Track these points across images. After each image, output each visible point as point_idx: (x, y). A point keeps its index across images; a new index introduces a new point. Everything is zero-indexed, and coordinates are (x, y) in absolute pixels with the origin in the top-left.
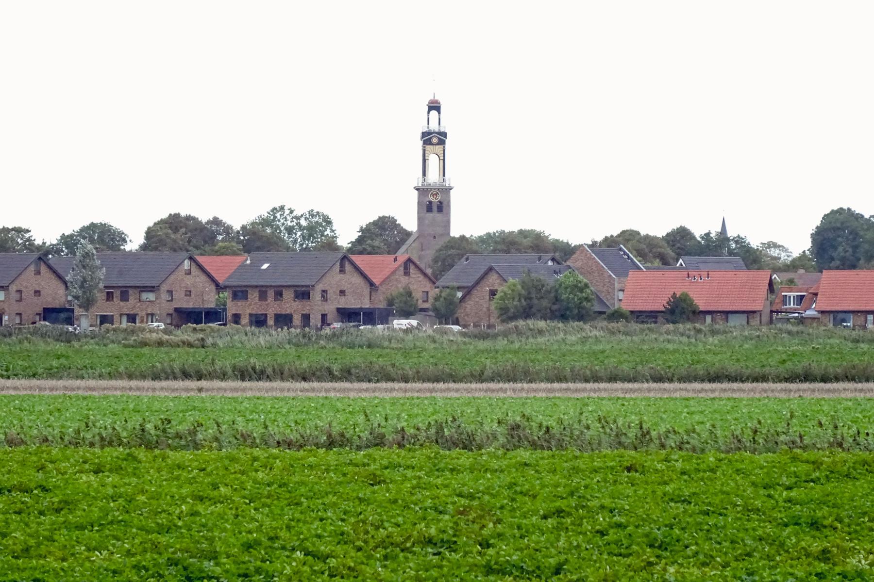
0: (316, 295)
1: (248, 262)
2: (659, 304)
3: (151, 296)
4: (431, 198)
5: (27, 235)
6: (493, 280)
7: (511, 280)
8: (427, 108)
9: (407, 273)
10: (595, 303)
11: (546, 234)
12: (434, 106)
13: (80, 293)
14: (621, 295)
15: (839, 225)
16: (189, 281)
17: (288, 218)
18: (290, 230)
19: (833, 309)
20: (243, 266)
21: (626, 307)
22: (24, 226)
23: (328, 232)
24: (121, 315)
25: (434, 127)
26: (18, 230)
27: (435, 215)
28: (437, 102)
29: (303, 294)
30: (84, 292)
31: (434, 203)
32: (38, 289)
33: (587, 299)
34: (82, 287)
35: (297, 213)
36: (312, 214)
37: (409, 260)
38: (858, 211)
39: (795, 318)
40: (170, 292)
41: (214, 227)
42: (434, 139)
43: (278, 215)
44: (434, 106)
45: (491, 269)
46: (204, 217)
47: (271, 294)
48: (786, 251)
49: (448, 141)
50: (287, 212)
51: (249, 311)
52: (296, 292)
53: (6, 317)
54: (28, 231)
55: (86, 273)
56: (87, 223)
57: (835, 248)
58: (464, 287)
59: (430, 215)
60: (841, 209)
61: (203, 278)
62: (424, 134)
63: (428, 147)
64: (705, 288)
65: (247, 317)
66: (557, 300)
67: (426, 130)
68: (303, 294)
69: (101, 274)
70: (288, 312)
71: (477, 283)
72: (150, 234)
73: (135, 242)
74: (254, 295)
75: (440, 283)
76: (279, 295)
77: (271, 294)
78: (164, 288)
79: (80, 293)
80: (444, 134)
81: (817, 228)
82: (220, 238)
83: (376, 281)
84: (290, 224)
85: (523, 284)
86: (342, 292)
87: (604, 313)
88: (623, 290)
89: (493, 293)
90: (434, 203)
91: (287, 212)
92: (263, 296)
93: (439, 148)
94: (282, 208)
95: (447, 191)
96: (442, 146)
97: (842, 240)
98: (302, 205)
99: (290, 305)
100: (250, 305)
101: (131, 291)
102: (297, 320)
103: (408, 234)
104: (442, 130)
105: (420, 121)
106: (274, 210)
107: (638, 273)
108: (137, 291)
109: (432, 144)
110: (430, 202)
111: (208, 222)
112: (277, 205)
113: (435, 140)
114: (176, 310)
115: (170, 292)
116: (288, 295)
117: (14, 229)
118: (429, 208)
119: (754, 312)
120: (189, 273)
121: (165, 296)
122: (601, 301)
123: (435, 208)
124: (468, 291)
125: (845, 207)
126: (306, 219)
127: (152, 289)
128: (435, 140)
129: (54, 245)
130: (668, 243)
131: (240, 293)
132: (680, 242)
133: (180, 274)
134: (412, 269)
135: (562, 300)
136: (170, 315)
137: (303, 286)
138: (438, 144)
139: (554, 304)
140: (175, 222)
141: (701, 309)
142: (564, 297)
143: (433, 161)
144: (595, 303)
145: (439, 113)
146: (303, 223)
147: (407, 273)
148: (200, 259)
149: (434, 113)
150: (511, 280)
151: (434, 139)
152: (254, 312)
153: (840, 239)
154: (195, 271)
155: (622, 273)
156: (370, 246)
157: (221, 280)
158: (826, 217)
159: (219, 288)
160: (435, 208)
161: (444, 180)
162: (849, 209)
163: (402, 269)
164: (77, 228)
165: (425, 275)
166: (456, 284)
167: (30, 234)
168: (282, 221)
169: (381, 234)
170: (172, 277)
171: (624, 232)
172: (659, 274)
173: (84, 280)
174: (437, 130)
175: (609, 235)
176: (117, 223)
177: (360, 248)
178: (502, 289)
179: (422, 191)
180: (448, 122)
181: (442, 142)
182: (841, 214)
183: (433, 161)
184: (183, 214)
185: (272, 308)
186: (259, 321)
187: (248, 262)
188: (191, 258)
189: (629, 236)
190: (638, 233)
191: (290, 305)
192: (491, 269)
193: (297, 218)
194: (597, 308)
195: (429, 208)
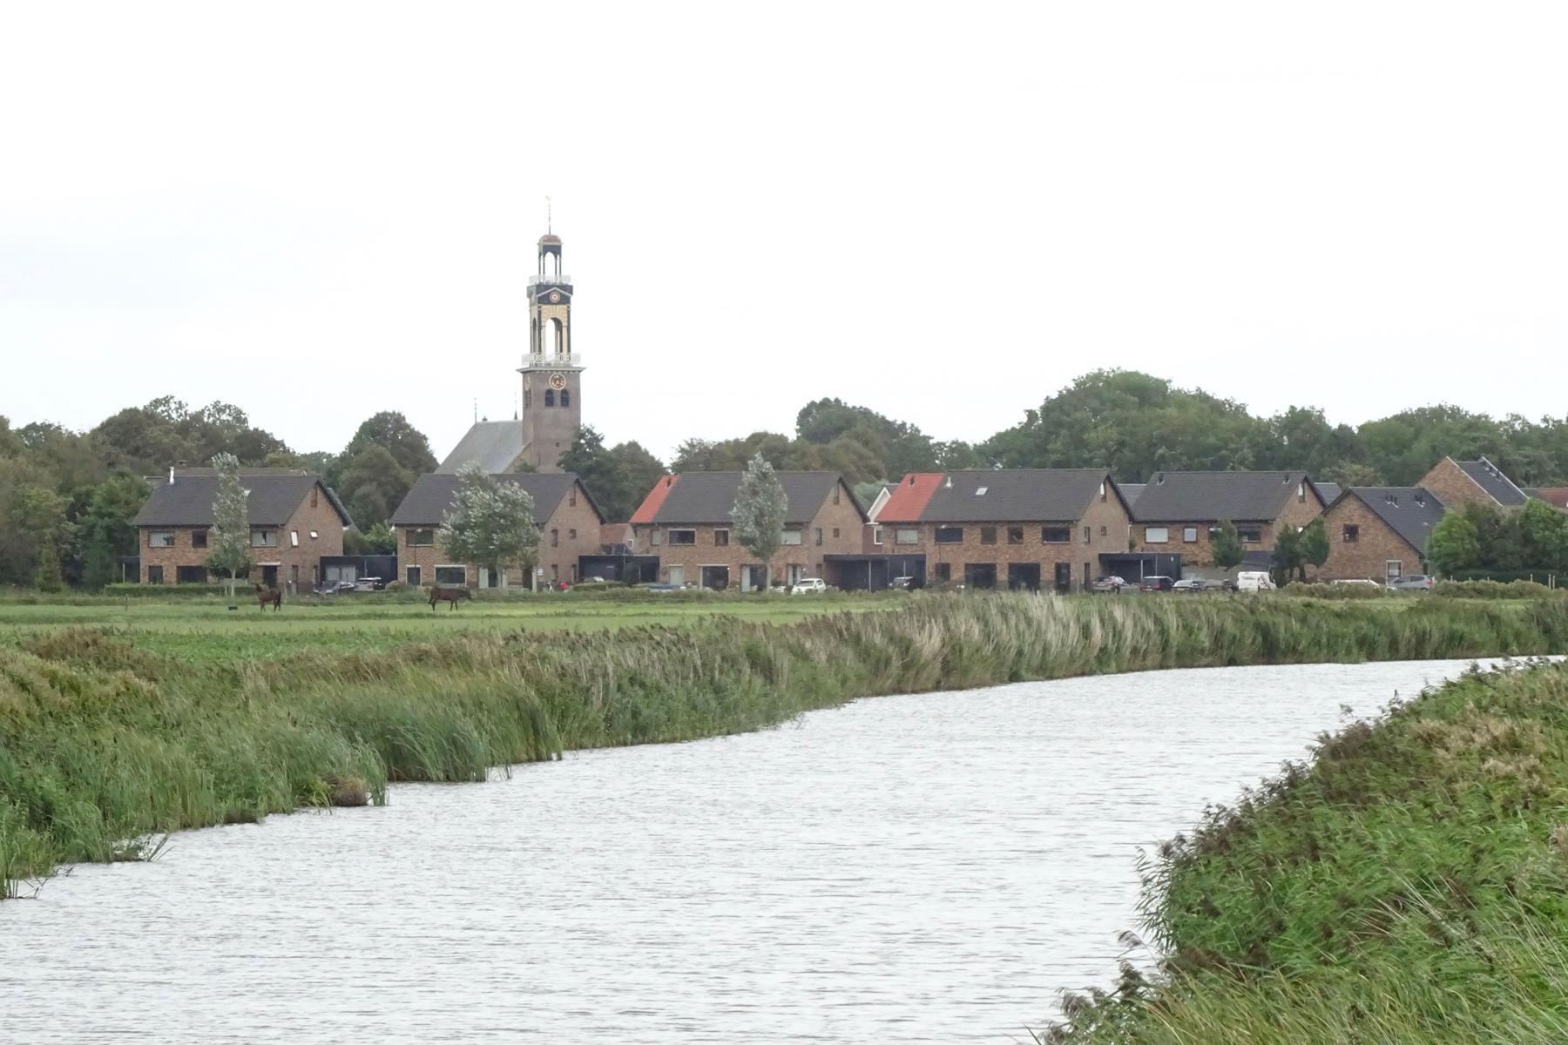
0: (1077, 534)
1: (949, 485)
4: (552, 385)
8: (536, 250)
12: (551, 247)
20: (941, 491)
24: (742, 566)
25: (550, 276)
27: (557, 411)
28: (555, 239)
29: (1057, 533)
30: (762, 533)
31: (552, 392)
34: (758, 524)
38: (1220, 395)
42: (550, 297)
44: (551, 247)
47: (1002, 533)
51: (964, 560)
53: (540, 572)
59: (551, 410)
65: (962, 568)
66: (1527, 540)
68: (1057, 533)
70: (1032, 560)
73: (791, 434)
74: (973, 536)
76: (1016, 535)
78: (814, 525)
80: (569, 289)
83: (1328, 502)
90: (552, 392)
92: (989, 537)
94: (166, 401)
95: (574, 374)
99: (1034, 549)
100: (967, 550)
101: (1026, 530)
102: (1047, 573)
105: (528, 268)
106: (157, 403)
109: (550, 303)
110: (550, 392)
113: (555, 297)
114: (827, 558)
115: (555, 531)
116: (1033, 536)
123: (558, 400)
128: (555, 297)
131: (949, 533)
133: (1294, 501)
135: (1534, 541)
136: (819, 566)
137: (1057, 522)
139: (1524, 546)
142: (1536, 536)
151: (550, 297)
152: (973, 561)
160: (558, 400)
162: (837, 400)
180: (572, 268)
181: (565, 300)
185: (1003, 555)
186: (982, 577)
191: (1034, 549)
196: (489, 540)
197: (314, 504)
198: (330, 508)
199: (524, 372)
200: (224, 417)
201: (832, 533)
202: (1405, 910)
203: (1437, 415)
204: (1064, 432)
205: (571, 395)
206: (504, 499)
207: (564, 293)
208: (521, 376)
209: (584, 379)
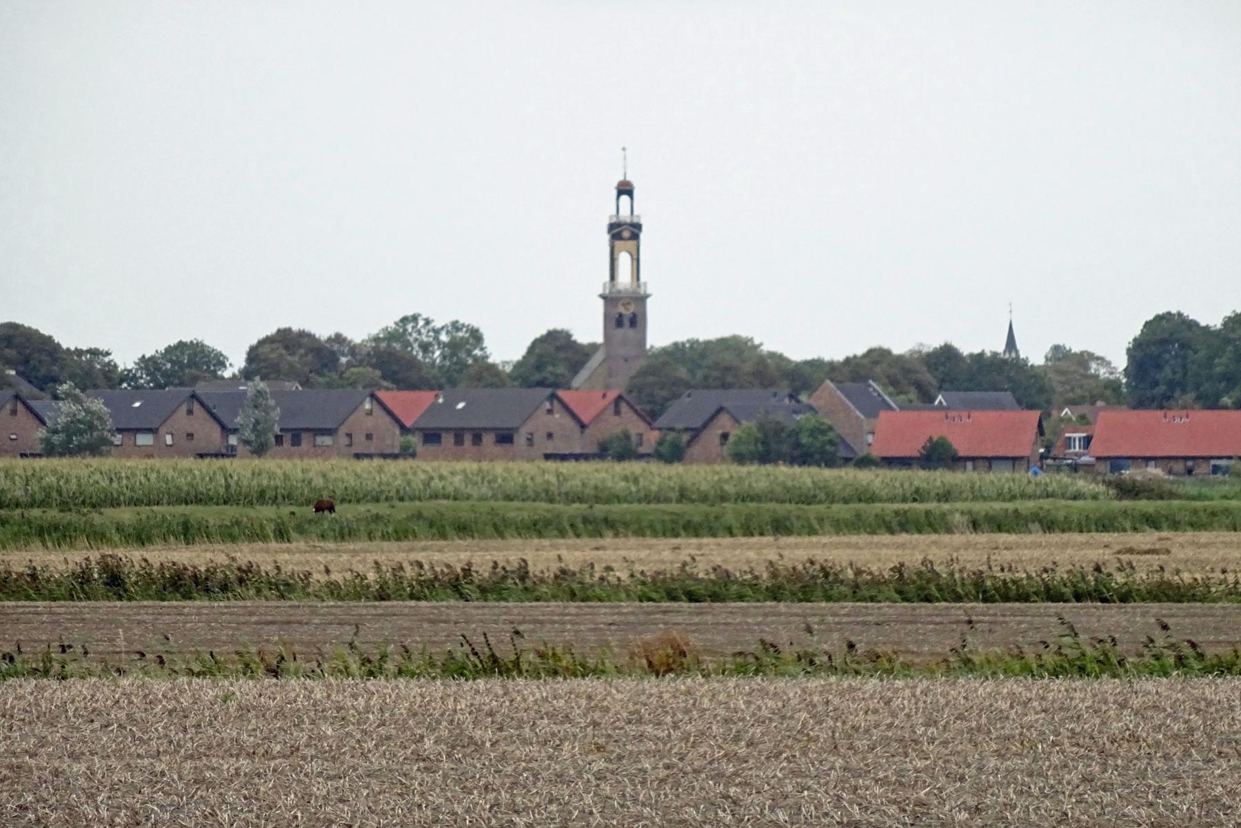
1: (441, 400)
2: (913, 448)
3: (327, 440)
4: (621, 310)
5: (107, 359)
6: (724, 422)
7: (745, 423)
8: (615, 193)
9: (617, 412)
10: (841, 448)
11: (757, 342)
12: (625, 189)
13: (253, 437)
14: (870, 438)
15: (1166, 336)
16: (369, 423)
17: (423, 331)
18: (425, 347)
19: (1112, 454)
20: (434, 405)
21: (876, 453)
22: (103, 347)
23: (477, 352)
26: (94, 352)
27: (626, 331)
30: (257, 436)
31: (625, 312)
32: (190, 431)
33: (831, 442)
35: (438, 324)
36: (456, 326)
37: (620, 398)
39: (1068, 465)
40: (349, 435)
41: (336, 347)
42: (624, 233)
43: (409, 327)
44: (625, 189)
45: (720, 410)
46: (323, 332)
47: (468, 438)
48: (1109, 363)
49: (642, 236)
50: (421, 323)
52: (497, 436)
54: (108, 354)
55: (259, 414)
56: (173, 342)
57: (1159, 367)
58: (692, 429)
59: (620, 332)
60: (1169, 313)
61: (388, 419)
62: (612, 227)
63: (618, 243)
64: (967, 428)
67: (614, 220)
69: (276, 414)
71: (705, 425)
72: (254, 355)
73: (236, 362)
75: (663, 421)
77: (468, 438)
78: (343, 430)
79: (253, 437)
81: (1135, 340)
82: (343, 360)
83: (585, 418)
84: (425, 339)
85: (761, 427)
86: (550, 436)
87: (851, 459)
88: (873, 433)
89: (725, 436)
90: (625, 312)
91: (421, 323)
93: (632, 243)
94: (415, 318)
95: (641, 300)
96: (634, 242)
97: (1174, 359)
98: (442, 312)
101: (304, 435)
103: (586, 352)
104: (635, 220)
105: (607, 208)
106: (405, 320)
107: (890, 413)
108: (311, 434)
110: (621, 315)
111: (330, 339)
112: (410, 313)
113: (626, 234)
115: (349, 435)
117: (90, 351)
118: (619, 322)
119: (1022, 458)
120: (370, 413)
121: (344, 440)
122: (848, 447)
123: (626, 322)
124: (696, 433)
125: (1174, 311)
126: (448, 332)
127: (329, 432)
128: (626, 234)
129: (130, 371)
130: (929, 367)
132: (944, 373)
133: (359, 414)
134: (624, 407)
138: (630, 239)
140: (287, 340)
141: (961, 454)
143: (624, 260)
144: (841, 448)
145: (632, 198)
146: (444, 338)
147: (617, 412)
148: (381, 394)
149: (625, 199)
150: (745, 423)
151: (624, 233)
153: (1167, 356)
154: (378, 411)
155: (871, 413)
156: (552, 373)
157: (408, 424)
158: (1148, 324)
159: (404, 429)
160: (626, 322)
161: (639, 286)
162: (1180, 314)
163: (612, 406)
164: (162, 349)
165: (636, 411)
166: (679, 426)
167: (111, 357)
168: (415, 335)
169: (554, 356)
170: (352, 418)
171: (871, 352)
172: (912, 415)
173: (257, 422)
174: (628, 220)
175: (851, 355)
176: (213, 342)
177: (537, 377)
178: (735, 433)
179: (610, 300)
180: (644, 208)
181: (635, 237)
182: (1168, 321)
183: (624, 260)
184: (295, 328)
187: (441, 400)
188: (373, 396)
189: (878, 356)
190: (888, 352)
192: (720, 410)
193: (437, 332)
194: (842, 453)
195: (619, 322)
196: (70, 441)
197: (14, 412)
198: (31, 416)
199: (603, 297)
200: (460, 334)
201: (363, 438)
202: (436, 742)
203: (736, 347)
204: (1230, 348)
205: (639, 320)
206: (88, 411)
207: (634, 230)
208: (601, 302)
209: (650, 303)
